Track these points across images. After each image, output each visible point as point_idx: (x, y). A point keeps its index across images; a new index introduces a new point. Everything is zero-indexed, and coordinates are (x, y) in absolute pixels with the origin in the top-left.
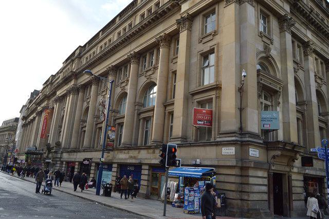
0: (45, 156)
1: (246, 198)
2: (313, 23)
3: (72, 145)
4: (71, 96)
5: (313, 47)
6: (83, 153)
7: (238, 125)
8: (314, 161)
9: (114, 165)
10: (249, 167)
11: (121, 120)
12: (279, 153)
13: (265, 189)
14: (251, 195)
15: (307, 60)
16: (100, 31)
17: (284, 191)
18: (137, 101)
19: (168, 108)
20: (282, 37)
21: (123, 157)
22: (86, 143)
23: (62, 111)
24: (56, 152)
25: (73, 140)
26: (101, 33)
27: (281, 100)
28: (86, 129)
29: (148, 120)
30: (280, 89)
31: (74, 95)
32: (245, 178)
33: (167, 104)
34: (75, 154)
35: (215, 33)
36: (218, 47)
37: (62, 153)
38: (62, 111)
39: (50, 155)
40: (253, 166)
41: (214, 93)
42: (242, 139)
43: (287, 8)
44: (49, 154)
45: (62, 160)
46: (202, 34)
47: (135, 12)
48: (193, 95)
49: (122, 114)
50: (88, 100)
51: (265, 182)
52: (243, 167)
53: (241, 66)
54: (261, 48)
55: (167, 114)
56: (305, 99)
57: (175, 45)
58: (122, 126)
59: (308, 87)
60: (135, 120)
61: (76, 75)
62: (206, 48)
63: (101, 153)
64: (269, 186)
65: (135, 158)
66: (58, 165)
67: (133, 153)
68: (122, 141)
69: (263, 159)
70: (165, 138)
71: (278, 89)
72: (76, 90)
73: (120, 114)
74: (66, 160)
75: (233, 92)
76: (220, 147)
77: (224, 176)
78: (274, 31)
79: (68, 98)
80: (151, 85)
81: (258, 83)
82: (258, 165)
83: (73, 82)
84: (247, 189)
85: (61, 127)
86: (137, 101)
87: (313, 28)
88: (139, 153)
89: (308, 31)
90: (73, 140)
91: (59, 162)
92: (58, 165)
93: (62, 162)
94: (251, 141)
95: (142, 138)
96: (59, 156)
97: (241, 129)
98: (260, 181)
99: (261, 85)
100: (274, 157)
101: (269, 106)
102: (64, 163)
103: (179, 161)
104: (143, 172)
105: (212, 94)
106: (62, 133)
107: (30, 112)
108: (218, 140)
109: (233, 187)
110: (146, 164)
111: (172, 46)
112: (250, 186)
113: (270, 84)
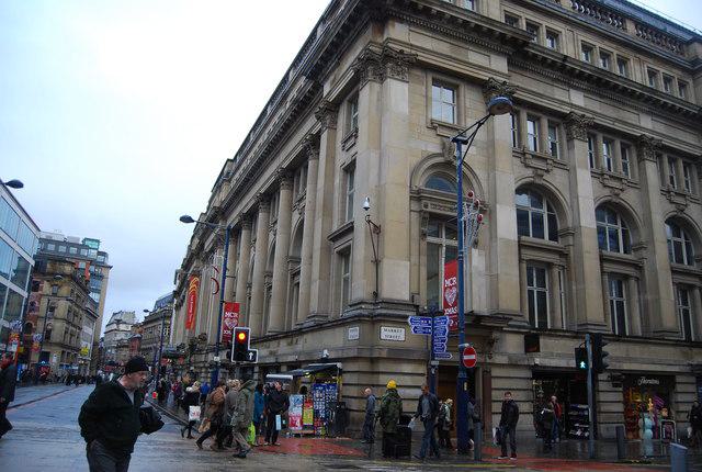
2: (581, 76)
15: (571, 147)
23: (271, 234)
32: (376, 376)
38: (271, 234)
42: (378, 312)
43: (499, 64)
50: (302, 204)
51: (422, 381)
59: (575, 200)
77: (520, 387)
82: (398, 355)
86: (291, 254)
87: (584, 85)
89: (572, 92)
94: (385, 315)
97: (376, 294)
99: (427, 216)
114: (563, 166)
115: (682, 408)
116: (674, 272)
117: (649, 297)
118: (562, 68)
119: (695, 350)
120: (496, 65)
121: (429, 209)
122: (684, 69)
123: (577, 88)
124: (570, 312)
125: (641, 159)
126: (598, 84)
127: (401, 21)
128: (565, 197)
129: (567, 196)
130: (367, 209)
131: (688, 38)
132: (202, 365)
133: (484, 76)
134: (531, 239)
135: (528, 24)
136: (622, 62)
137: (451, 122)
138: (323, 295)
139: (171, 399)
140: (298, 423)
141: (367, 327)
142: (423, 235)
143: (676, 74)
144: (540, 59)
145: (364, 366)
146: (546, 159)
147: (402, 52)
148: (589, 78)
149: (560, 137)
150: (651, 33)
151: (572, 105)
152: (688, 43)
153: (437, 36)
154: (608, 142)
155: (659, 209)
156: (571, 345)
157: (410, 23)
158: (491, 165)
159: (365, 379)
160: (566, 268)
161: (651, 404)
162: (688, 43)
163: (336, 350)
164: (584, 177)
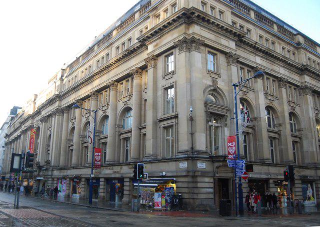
0: (35, 174)
1: (196, 197)
2: (261, 51)
3: (62, 162)
4: (57, 117)
5: (285, 80)
6: (73, 170)
7: (191, 146)
8: (254, 167)
9: (101, 180)
10: (197, 176)
11: (104, 140)
12: (221, 164)
13: (211, 190)
14: (200, 195)
16: (81, 56)
17: (230, 192)
18: (117, 123)
19: (143, 131)
21: (107, 172)
22: (74, 160)
23: (49, 131)
24: (47, 169)
25: (62, 158)
26: (81, 58)
27: (228, 122)
28: (74, 147)
29: (127, 139)
30: (226, 113)
33: (141, 128)
34: (66, 171)
36: (176, 84)
37: (52, 171)
39: (41, 173)
40: (200, 174)
41: (173, 120)
42: (192, 156)
43: (232, 45)
44: (40, 171)
45: (53, 177)
46: (165, 72)
47: (111, 44)
48: (160, 121)
49: (105, 135)
50: (73, 121)
51: (212, 185)
52: (193, 175)
55: (142, 136)
56: (256, 116)
58: (106, 145)
60: (117, 140)
62: (168, 83)
63: (90, 169)
64: (214, 188)
65: (118, 173)
66: (50, 182)
67: (116, 169)
68: (107, 158)
70: (141, 156)
73: (103, 134)
74: (57, 177)
75: (186, 121)
76: (177, 162)
78: (222, 66)
79: (53, 119)
80: (128, 109)
81: (206, 112)
82: (204, 174)
83: (57, 104)
85: (49, 146)
87: (261, 54)
88: (121, 168)
89: (256, 57)
90: (62, 158)
91: (50, 179)
92: (50, 182)
93: (53, 179)
95: (123, 155)
96: (50, 173)
97: (192, 148)
98: (207, 185)
99: (209, 113)
100: (218, 167)
101: (274, 138)
102: (83, 180)
103: (146, 174)
105: (173, 121)
106: (50, 152)
107: (12, 130)
108: (177, 157)
109: (186, 190)
110: (127, 177)
112: (198, 189)
113: (218, 110)
114: (252, 90)
115: (297, 194)
116: (268, 131)
117: (283, 147)
118: (254, 47)
119: (301, 169)
120: (230, 45)
121: (210, 110)
122: (295, 47)
123: (258, 56)
124: (256, 154)
125: (280, 86)
126: (267, 54)
127: (198, 24)
128: (253, 103)
129: (254, 102)
130: (191, 111)
131: (295, 33)
132: (50, 177)
133: (228, 51)
134: (272, 128)
135: (240, 26)
136: (273, 43)
137: (213, 70)
138: (155, 146)
139: (102, 192)
140: (160, 205)
141: (190, 162)
142: (208, 121)
143: (292, 48)
144: (221, 26)
145: (189, 179)
146: (247, 87)
147: (199, 39)
148: (263, 52)
149: (296, 94)
150: (244, 8)
151: (257, 63)
152: (295, 35)
153: (210, 32)
154: (290, 87)
155: (262, 102)
156: (282, 170)
157: (201, 26)
158: (257, 98)
159: (191, 185)
160: (255, 135)
161: (285, 193)
162: (295, 35)
163: (172, 172)
164: (261, 95)
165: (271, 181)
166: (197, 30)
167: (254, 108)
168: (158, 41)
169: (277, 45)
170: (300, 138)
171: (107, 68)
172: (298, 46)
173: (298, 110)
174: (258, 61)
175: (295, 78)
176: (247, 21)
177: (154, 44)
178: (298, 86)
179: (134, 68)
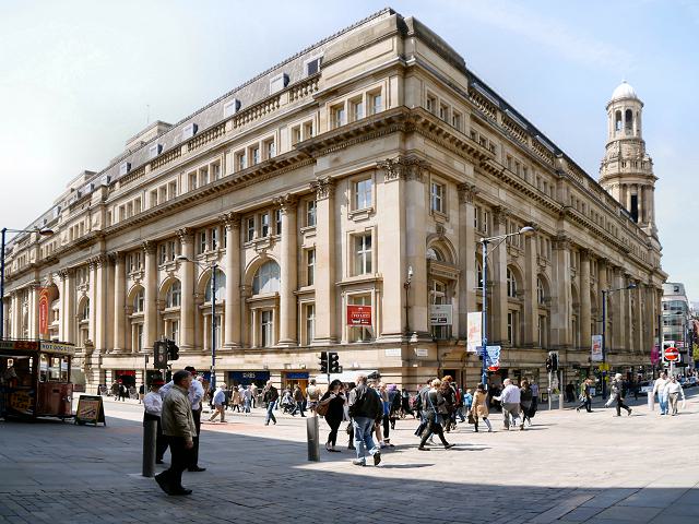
4: (99, 271)
20: (462, 210)
27: (457, 289)
31: (104, 266)
35: (372, 212)
43: (470, 170)
53: (406, 261)
54: (433, 230)
57: (305, 209)
59: (496, 266)
61: (104, 236)
69: (433, 356)
71: (453, 278)
72: (109, 261)
79: (92, 273)
82: (426, 363)
84: (406, 380)
104: (108, 375)
111: (301, 210)
123: (503, 188)
124: (522, 336)
128: (523, 271)
143: (548, 179)
151: (501, 201)
154: (513, 224)
156: (63, 335)
157: (427, 137)
160: (522, 314)
165: (510, 371)
166: (419, 145)
167: (524, 279)
168: (339, 154)
169: (530, 171)
170: (549, 312)
171: (218, 190)
172: (558, 175)
173: (548, 272)
174: (502, 196)
175: (551, 226)
176: (492, 131)
177: (334, 156)
178: (552, 237)
179: (285, 194)
